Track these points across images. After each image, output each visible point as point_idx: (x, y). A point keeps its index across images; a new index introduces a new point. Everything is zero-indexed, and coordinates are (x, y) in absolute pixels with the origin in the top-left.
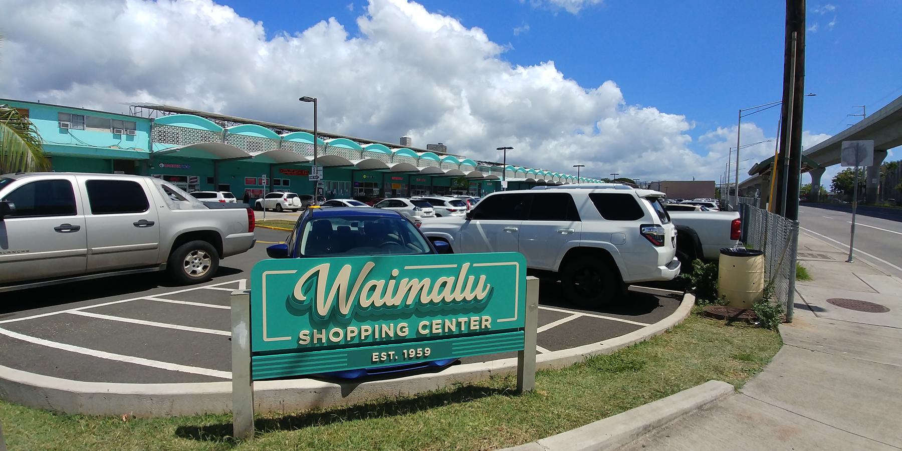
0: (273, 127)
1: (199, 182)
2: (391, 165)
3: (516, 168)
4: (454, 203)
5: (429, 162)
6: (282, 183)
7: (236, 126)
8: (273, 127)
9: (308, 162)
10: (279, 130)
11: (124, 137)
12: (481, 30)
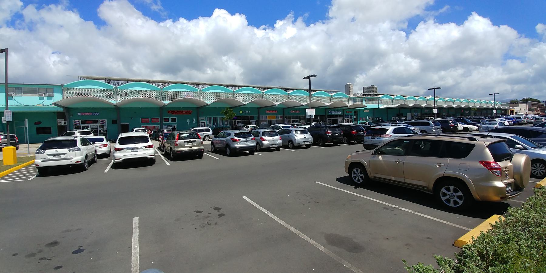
0: (283, 89)
1: (106, 124)
2: (445, 106)
3: (427, 98)
4: (236, 135)
5: (217, 95)
6: (170, 120)
7: (291, 91)
8: (283, 89)
9: (244, 105)
10: (287, 90)
11: (46, 98)
12: (505, 26)
